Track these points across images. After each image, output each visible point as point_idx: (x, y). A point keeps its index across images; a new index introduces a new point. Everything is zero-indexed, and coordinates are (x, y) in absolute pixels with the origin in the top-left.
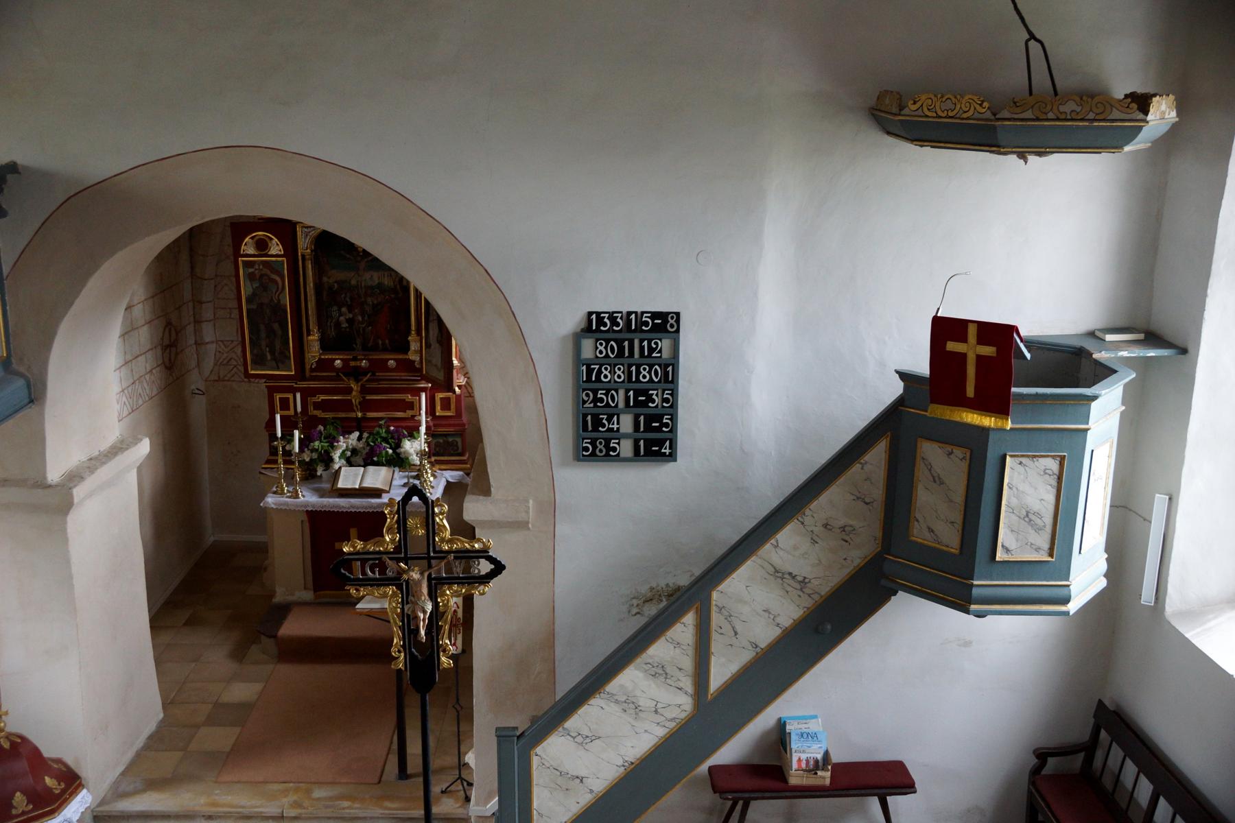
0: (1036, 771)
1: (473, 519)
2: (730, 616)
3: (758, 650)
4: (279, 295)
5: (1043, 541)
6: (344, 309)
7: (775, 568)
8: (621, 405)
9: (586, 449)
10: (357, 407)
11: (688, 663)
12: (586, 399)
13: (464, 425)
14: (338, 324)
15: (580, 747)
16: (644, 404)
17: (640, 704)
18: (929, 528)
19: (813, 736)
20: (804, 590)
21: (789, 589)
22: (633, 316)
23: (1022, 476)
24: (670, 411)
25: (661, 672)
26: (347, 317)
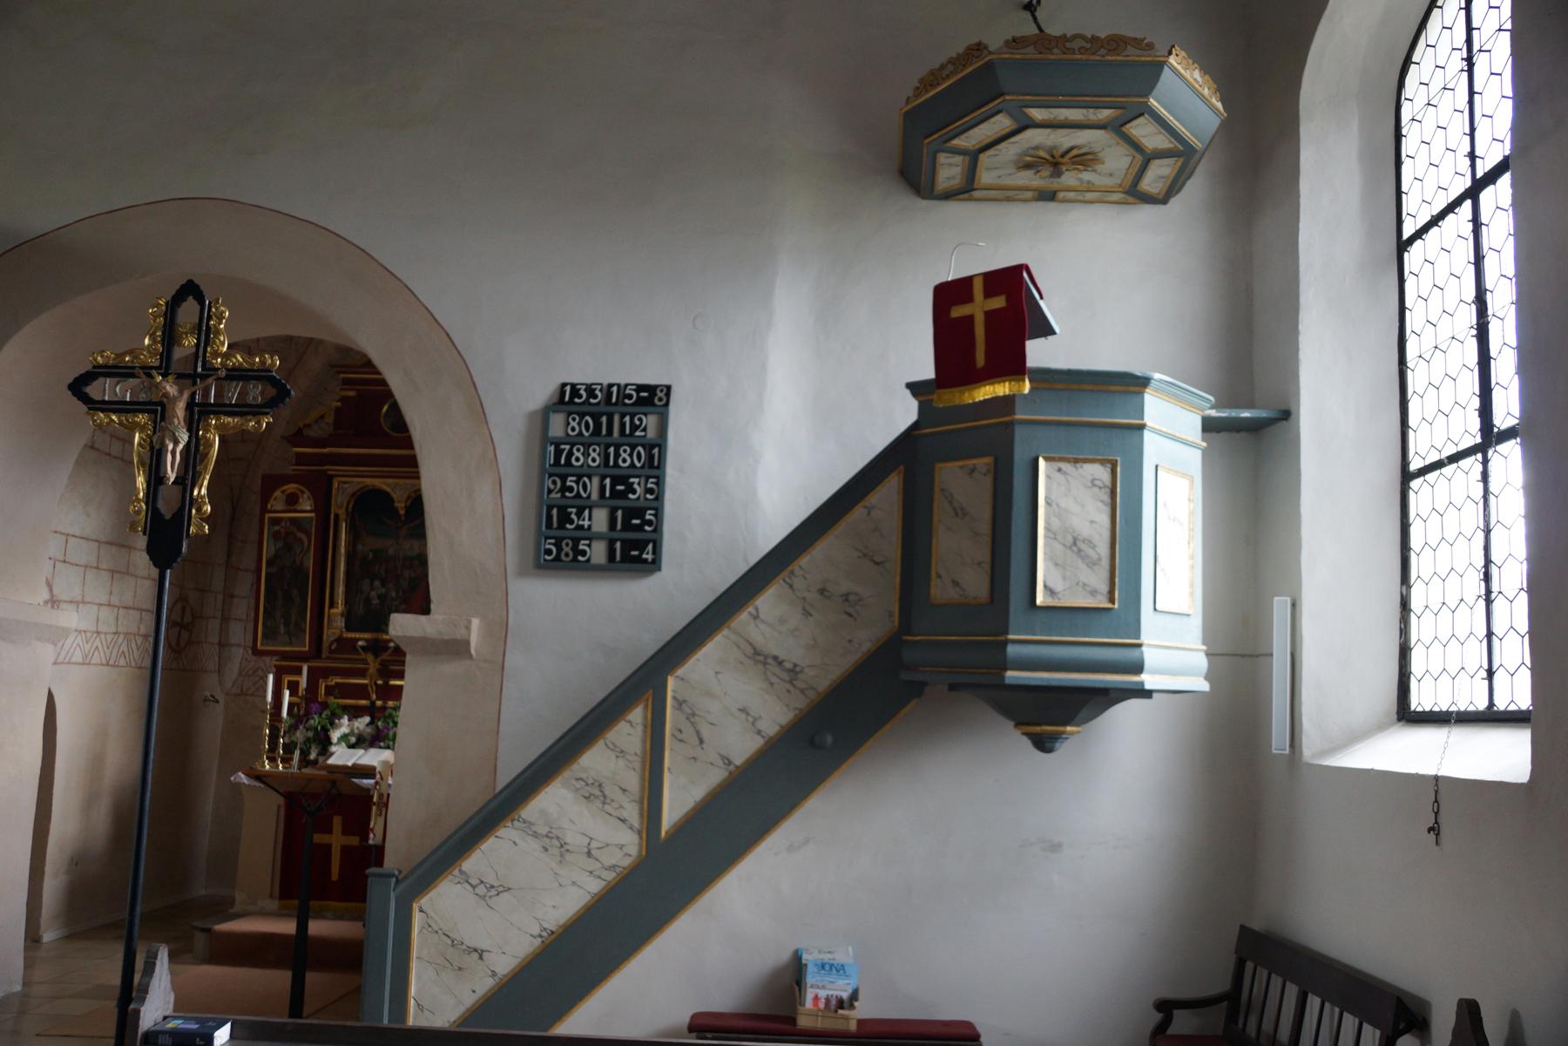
0: (1160, 1029)
1: (400, 634)
2: (694, 715)
3: (732, 768)
5: (1099, 581)
7: (754, 649)
8: (595, 496)
10: (372, 687)
11: (633, 781)
12: (552, 487)
14: (368, 600)
15: (482, 902)
16: (623, 495)
17: (568, 841)
18: (954, 582)
19: (840, 969)
20: (795, 682)
21: (774, 680)
22: (615, 389)
23: (1063, 488)
24: (655, 504)
25: (597, 792)
26: (379, 592)
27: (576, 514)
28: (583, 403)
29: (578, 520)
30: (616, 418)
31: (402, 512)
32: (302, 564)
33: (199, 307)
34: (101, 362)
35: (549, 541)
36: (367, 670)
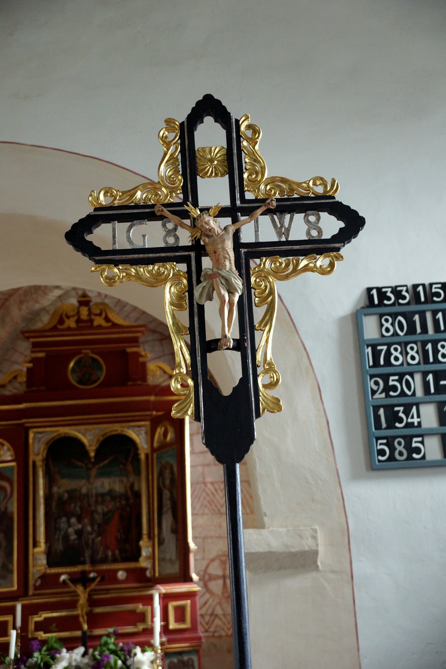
4: (6, 503)
6: (73, 520)
8: (420, 393)
9: (382, 452)
10: (83, 617)
12: (375, 388)
13: (199, 638)
14: (66, 537)
22: (420, 289)
27: (404, 412)
28: (393, 304)
29: (407, 418)
30: (429, 316)
31: (92, 454)
32: (6, 509)
33: (224, 132)
34: (104, 203)
35: (380, 441)
36: (77, 601)
